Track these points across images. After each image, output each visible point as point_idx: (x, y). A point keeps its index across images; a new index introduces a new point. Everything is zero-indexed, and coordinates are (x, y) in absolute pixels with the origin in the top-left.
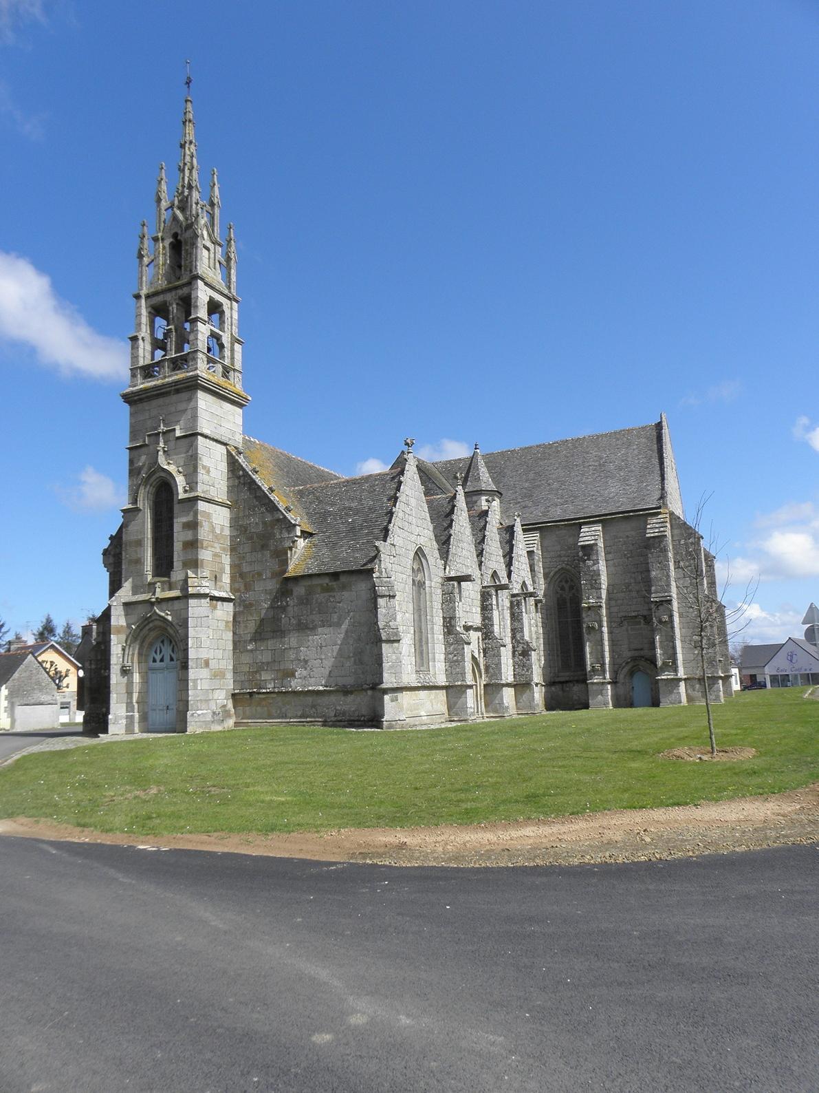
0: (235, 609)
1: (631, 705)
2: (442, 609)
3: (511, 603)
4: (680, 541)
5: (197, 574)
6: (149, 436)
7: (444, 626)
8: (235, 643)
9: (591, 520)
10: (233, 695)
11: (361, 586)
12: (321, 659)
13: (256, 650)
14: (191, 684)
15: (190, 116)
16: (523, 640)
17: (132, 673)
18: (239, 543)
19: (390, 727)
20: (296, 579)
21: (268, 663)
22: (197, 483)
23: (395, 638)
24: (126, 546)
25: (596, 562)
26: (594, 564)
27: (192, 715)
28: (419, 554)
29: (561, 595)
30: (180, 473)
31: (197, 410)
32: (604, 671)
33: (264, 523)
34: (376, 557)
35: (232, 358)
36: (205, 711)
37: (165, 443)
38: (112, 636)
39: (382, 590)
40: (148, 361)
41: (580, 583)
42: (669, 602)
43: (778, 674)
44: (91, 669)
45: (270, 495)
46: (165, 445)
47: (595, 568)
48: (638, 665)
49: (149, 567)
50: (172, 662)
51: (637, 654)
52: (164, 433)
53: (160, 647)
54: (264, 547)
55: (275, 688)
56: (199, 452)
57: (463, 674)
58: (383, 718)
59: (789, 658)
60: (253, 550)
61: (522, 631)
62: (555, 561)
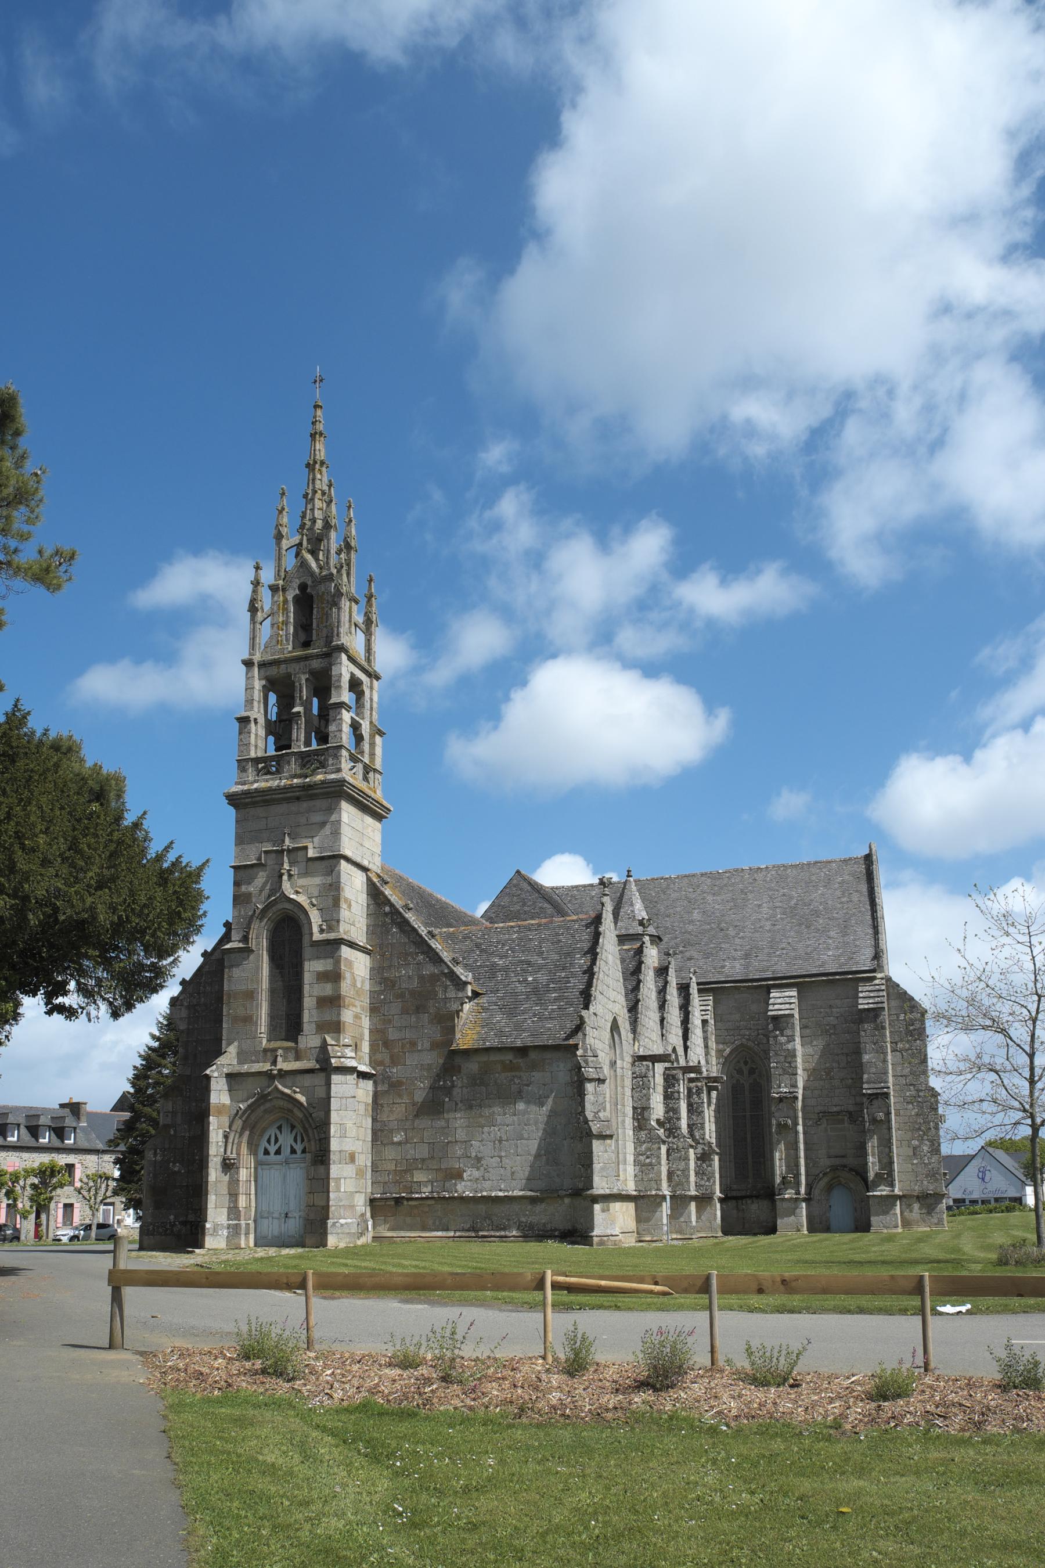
1: (827, 1229)
2: (632, 1097)
3: (689, 1090)
4: (898, 1015)
5: (338, 1040)
6: (266, 852)
7: (634, 1119)
8: (374, 1132)
9: (783, 982)
10: (372, 1201)
11: (560, 1070)
12: (500, 1157)
13: (407, 1142)
14: (332, 1184)
15: (320, 427)
16: (703, 1139)
17: (238, 1168)
18: (383, 1002)
19: (601, 1243)
20: (466, 1053)
21: (423, 1160)
22: (338, 921)
23: (608, 1133)
25: (791, 1039)
26: (789, 1041)
27: (334, 1224)
28: (615, 1027)
29: (738, 1080)
30: (314, 905)
31: (340, 824)
32: (798, 1184)
33: (421, 978)
34: (579, 1028)
35: (372, 755)
36: (349, 1221)
37: (291, 864)
38: (211, 1117)
39: (590, 1072)
40: (260, 754)
41: (769, 1066)
42: (886, 1095)
43: (964, 1197)
45: (429, 942)
46: (290, 866)
47: (790, 1046)
48: (839, 1177)
49: (263, 1027)
50: (294, 1156)
51: (838, 1161)
52: (289, 851)
53: (276, 1136)
54: (419, 1009)
55: (432, 1192)
56: (342, 881)
57: (658, 1181)
58: (592, 1229)
59: (980, 1175)
60: (405, 1011)
61: (703, 1128)
62: (733, 1035)
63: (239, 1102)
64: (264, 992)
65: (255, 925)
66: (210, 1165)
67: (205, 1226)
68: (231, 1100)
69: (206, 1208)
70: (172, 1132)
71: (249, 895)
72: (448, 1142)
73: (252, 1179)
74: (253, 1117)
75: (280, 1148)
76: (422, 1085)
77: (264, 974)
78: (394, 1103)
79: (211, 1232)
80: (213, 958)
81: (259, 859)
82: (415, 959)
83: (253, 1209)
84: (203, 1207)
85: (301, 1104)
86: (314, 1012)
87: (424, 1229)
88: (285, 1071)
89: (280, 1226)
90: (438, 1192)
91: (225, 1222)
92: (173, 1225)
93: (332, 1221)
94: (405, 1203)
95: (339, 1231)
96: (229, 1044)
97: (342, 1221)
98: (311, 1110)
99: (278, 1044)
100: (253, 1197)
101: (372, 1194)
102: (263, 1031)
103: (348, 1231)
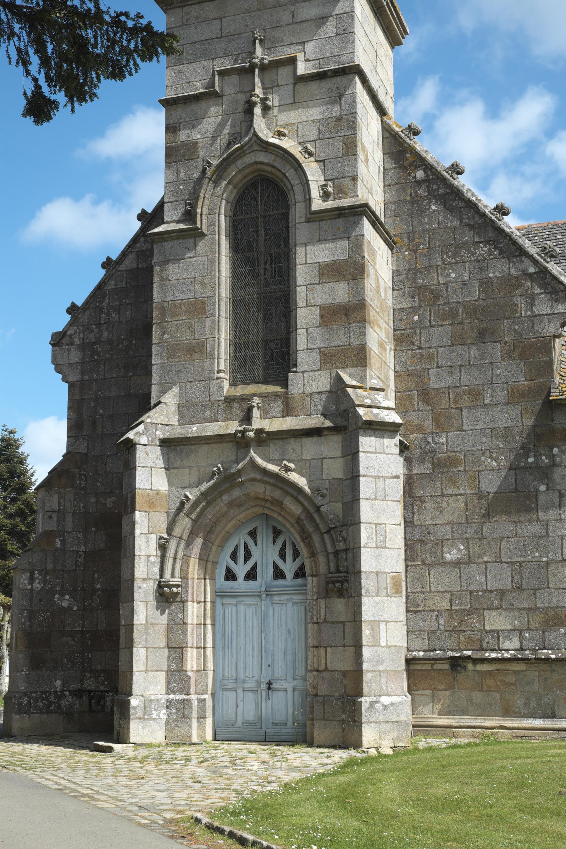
0: (409, 469)
5: (363, 378)
6: (222, 73)
13: (470, 561)
14: (366, 632)
17: (184, 602)
18: (418, 327)
21: (502, 593)
22: (354, 179)
24: (163, 315)
30: (310, 154)
38: (137, 513)
44: (32, 590)
50: (281, 582)
52: (263, 68)
55: (522, 649)
63: (183, 488)
64: (223, 304)
65: (207, 191)
66: (136, 595)
67: (128, 702)
68: (170, 484)
69: (131, 672)
70: (58, 545)
71: (193, 146)
72: (548, 563)
73: (209, 621)
74: (209, 515)
75: (254, 568)
76: (494, 464)
77: (223, 273)
78: (443, 495)
79: (139, 713)
80: (122, 267)
81: (211, 84)
82: (473, 254)
83: (210, 674)
84: (122, 666)
85: (299, 490)
86: (317, 333)
87: (507, 713)
88: (269, 433)
89: (257, 704)
90: (533, 650)
91: (163, 697)
92: (60, 696)
93: (368, 699)
94: (470, 666)
95: (381, 718)
96: (163, 392)
97: (385, 700)
98: (319, 501)
99: (251, 389)
100: (209, 652)
101: (409, 650)
102: (222, 367)
103: (396, 719)
